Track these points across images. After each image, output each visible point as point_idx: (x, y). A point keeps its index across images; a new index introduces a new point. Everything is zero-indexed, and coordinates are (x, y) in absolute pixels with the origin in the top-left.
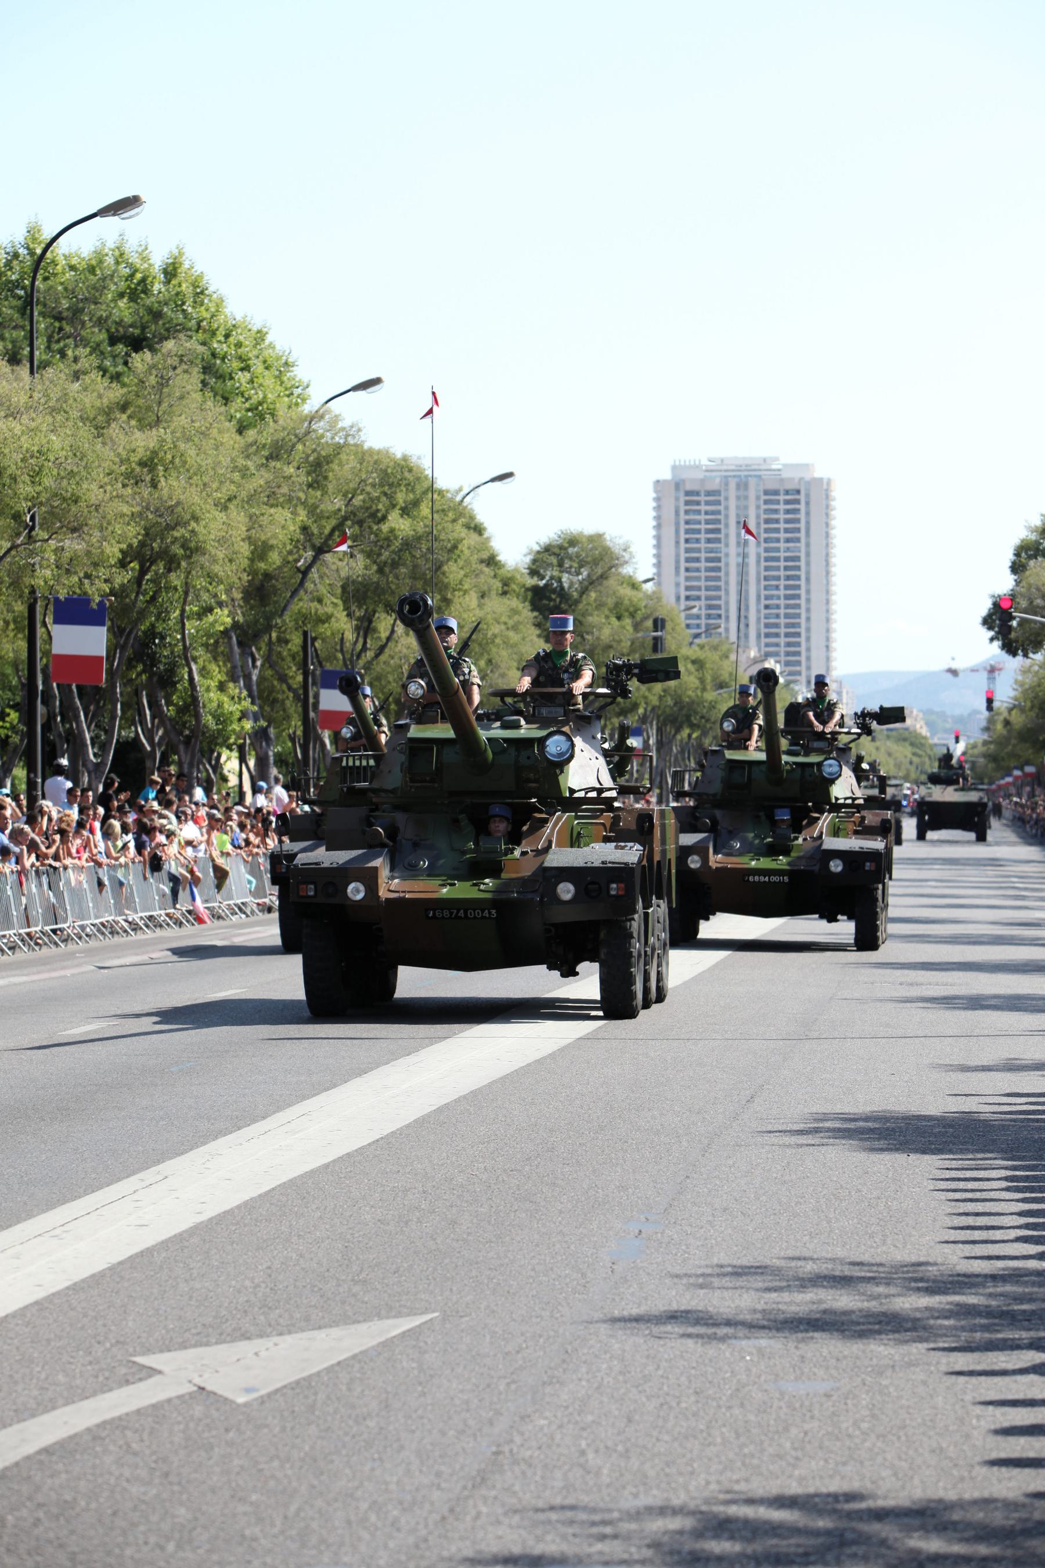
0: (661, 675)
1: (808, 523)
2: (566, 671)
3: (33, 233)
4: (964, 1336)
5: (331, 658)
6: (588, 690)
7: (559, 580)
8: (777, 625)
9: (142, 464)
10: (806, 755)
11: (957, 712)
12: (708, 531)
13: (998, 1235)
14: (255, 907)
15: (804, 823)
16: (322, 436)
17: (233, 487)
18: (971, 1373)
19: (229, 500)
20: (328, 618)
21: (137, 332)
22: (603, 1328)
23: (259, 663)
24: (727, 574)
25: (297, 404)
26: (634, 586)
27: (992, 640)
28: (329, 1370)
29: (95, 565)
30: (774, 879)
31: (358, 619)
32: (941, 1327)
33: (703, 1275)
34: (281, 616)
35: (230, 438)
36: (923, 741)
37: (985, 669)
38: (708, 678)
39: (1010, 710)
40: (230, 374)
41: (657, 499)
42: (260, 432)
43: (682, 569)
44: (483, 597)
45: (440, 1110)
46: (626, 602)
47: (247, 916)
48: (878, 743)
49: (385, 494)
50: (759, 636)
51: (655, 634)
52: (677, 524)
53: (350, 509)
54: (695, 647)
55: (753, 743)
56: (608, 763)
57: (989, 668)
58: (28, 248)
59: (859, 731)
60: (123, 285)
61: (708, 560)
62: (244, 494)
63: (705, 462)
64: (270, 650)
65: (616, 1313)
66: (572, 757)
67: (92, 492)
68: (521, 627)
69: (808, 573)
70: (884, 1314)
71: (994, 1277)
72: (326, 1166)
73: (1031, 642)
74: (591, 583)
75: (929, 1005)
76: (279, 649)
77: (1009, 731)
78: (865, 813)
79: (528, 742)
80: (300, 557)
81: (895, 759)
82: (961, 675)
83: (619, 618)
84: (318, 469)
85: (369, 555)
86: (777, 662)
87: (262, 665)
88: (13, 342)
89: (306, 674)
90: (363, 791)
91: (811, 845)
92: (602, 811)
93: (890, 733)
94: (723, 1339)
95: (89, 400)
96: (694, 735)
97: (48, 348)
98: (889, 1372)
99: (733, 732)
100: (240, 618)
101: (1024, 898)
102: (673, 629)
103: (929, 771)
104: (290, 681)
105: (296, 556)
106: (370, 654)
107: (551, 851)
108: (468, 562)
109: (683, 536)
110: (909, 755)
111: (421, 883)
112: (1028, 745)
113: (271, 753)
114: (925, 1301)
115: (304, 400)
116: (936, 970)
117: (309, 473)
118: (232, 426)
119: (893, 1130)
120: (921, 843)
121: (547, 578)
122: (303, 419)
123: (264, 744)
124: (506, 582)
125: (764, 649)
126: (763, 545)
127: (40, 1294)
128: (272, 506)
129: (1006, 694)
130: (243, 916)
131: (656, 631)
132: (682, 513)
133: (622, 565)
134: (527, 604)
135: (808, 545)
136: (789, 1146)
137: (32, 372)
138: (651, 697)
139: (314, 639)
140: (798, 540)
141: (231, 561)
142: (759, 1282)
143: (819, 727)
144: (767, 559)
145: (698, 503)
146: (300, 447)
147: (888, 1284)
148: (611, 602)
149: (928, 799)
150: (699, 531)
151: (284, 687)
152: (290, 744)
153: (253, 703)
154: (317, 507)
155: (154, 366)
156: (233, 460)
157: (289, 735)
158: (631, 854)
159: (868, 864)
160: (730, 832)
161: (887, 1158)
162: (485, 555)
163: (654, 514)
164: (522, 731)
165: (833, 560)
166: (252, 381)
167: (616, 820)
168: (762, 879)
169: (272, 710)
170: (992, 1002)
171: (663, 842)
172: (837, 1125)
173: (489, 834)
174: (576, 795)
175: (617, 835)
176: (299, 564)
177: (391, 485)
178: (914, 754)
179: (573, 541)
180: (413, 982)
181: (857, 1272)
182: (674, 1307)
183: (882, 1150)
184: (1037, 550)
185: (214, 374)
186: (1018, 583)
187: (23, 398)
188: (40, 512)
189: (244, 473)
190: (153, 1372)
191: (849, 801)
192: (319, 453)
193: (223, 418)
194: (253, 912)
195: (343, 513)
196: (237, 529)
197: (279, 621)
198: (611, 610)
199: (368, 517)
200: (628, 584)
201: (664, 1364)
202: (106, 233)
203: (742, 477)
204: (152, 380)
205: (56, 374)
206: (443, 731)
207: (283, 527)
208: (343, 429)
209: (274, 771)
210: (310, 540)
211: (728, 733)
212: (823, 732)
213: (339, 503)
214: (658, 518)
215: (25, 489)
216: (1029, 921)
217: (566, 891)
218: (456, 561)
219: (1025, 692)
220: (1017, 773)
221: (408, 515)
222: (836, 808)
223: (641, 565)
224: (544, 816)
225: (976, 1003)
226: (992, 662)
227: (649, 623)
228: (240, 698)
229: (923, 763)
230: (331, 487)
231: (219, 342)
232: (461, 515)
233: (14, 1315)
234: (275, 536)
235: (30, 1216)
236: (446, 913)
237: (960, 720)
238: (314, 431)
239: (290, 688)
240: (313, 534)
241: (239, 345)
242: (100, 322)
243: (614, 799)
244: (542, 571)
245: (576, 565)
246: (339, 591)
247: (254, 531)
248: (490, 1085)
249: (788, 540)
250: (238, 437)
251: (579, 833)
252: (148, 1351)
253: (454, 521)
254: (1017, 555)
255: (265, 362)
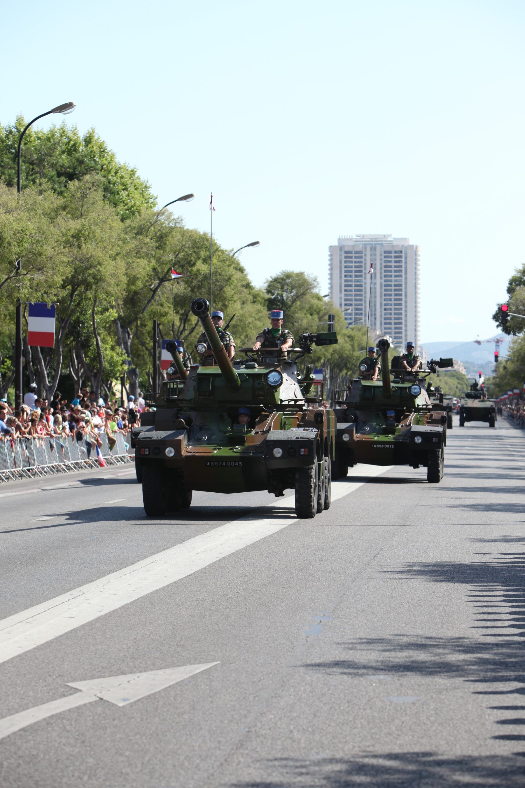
0: (327, 342)
1: (406, 268)
2: (279, 339)
3: (19, 121)
4: (482, 674)
5: (167, 334)
6: (290, 349)
7: (282, 296)
8: (390, 319)
9: (73, 236)
10: (403, 383)
11: (480, 362)
12: (356, 271)
13: (499, 624)
14: (129, 458)
15: (402, 417)
16: (163, 223)
17: (119, 248)
18: (486, 693)
19: (117, 255)
20: (166, 314)
21: (71, 171)
22: (302, 669)
23: (131, 336)
24: (365, 293)
25: (151, 207)
26: (319, 298)
27: (498, 326)
28: (165, 690)
29: (50, 287)
30: (386, 446)
31: (181, 314)
32: (471, 669)
33: (352, 643)
34: (142, 313)
35: (118, 224)
36: (463, 377)
37: (494, 341)
38: (356, 345)
39: (507, 361)
40: (118, 192)
41: (331, 255)
42: (132, 221)
43: (343, 290)
44: (243, 303)
45: (221, 560)
46: (315, 307)
47: (125, 463)
48: (440, 378)
49: (195, 252)
50: (381, 324)
51: (329, 323)
52: (341, 268)
53: (177, 259)
54: (349, 329)
55: (375, 377)
56: (300, 387)
57: (496, 341)
58: (17, 128)
59: (429, 371)
60: (64, 147)
61: (356, 286)
62: (124, 252)
63: (354, 237)
64: (137, 330)
65: (309, 662)
66: (281, 383)
67: (48, 250)
68: (262, 319)
69: (406, 292)
70: (442, 663)
71: (497, 645)
72: (164, 588)
73: (517, 327)
74: (297, 297)
75: (466, 509)
76: (141, 329)
77: (506, 372)
78: (432, 412)
79: (259, 376)
80: (152, 283)
81: (449, 385)
82: (482, 344)
83: (311, 315)
84: (161, 239)
85: (186, 282)
86: (390, 337)
87: (133, 337)
88: (9, 175)
89: (155, 342)
90: (174, 400)
91: (405, 429)
92: (297, 411)
93: (446, 373)
94: (362, 675)
95: (47, 205)
96: (349, 373)
97: (27, 178)
98: (445, 692)
99: (365, 371)
100: (122, 314)
101: (513, 455)
102: (338, 320)
103: (466, 392)
104: (147, 345)
105: (150, 283)
106: (187, 332)
107: (270, 432)
108: (236, 286)
109: (343, 274)
110: (456, 384)
111: (204, 448)
112: (515, 379)
113: (137, 381)
114: (463, 657)
115: (154, 205)
116: (469, 491)
117: (156, 242)
118: (118, 218)
119: (447, 571)
120: (462, 428)
121: (276, 294)
122: (154, 215)
123: (134, 377)
124: (255, 296)
125: (383, 331)
126: (384, 279)
127: (20, 651)
128: (138, 258)
129: (504, 353)
130: (123, 463)
131: (330, 321)
132: (343, 262)
133: (313, 288)
134: (265, 307)
135: (406, 278)
136: (395, 579)
137: (18, 191)
138: (327, 354)
139: (159, 325)
140: (401, 276)
141: (117, 285)
142: (380, 647)
143: (409, 369)
144: (385, 286)
145: (351, 257)
146: (152, 228)
147: (444, 648)
148: (307, 307)
149: (465, 406)
150: (351, 271)
151: (144, 348)
152: (147, 377)
153: (128, 356)
154: (161, 258)
155: (79, 188)
156: (119, 235)
157: (146, 373)
158: (311, 433)
159: (434, 439)
160: (364, 422)
161: (444, 585)
162: (244, 283)
163: (329, 263)
164: (256, 370)
165: (419, 286)
166: (128, 196)
167: (304, 416)
168: (380, 446)
169: (138, 360)
170: (497, 507)
171: (328, 427)
172: (419, 568)
173: (238, 423)
174: (284, 403)
175: (305, 424)
176: (152, 287)
177: (198, 248)
178: (458, 383)
179: (288, 276)
180: (200, 498)
181: (429, 642)
182: (338, 659)
183: (441, 581)
184: (521, 281)
185: (110, 192)
186: (511, 298)
187: (14, 204)
188: (22, 260)
189: (124, 241)
190: (77, 690)
191: (424, 407)
192: (162, 231)
193: (114, 214)
194: (128, 461)
195: (174, 262)
196: (121, 269)
197: (141, 315)
198: (307, 311)
199: (186, 264)
200: (316, 298)
201: (332, 688)
202: (55, 121)
203: (373, 244)
204: (79, 195)
205: (31, 191)
206: (215, 370)
207: (144, 268)
208: (174, 219)
209: (139, 391)
210: (157, 275)
211: (363, 372)
212: (411, 371)
213: (171, 257)
214: (331, 265)
215: (15, 249)
216: (516, 467)
217: (278, 452)
218: (230, 286)
219: (514, 352)
220: (510, 393)
221: (206, 263)
222: (418, 410)
223: (323, 288)
224: (267, 414)
225: (489, 508)
226: (498, 338)
227: (327, 317)
228: (122, 354)
229: (463, 388)
230: (168, 249)
231: (112, 176)
232: (233, 263)
233: (7, 662)
234: (139, 273)
235: (16, 612)
236: (216, 463)
237: (481, 366)
238: (159, 220)
239: (147, 349)
240: (158, 272)
241: (122, 177)
242: (53, 166)
243: (304, 405)
244: (273, 291)
245: (290, 288)
246: (172, 300)
247: (129, 271)
248: (246, 548)
249: (396, 276)
250: (121, 224)
251: (285, 423)
252: (74, 680)
253: (229, 266)
254: (511, 284)
255: (135, 186)
